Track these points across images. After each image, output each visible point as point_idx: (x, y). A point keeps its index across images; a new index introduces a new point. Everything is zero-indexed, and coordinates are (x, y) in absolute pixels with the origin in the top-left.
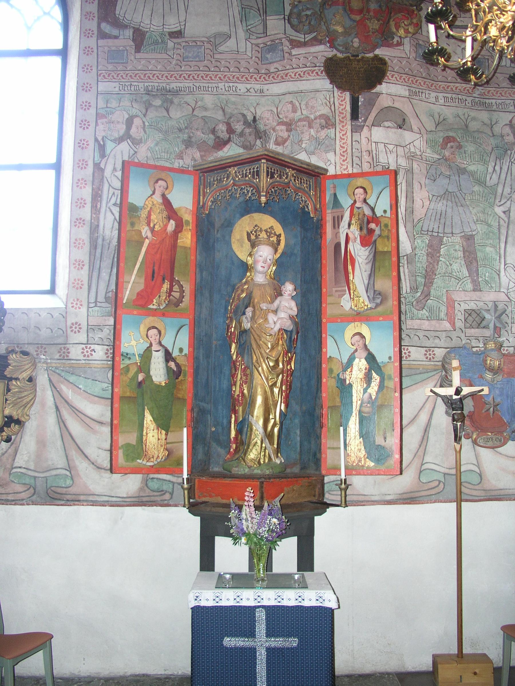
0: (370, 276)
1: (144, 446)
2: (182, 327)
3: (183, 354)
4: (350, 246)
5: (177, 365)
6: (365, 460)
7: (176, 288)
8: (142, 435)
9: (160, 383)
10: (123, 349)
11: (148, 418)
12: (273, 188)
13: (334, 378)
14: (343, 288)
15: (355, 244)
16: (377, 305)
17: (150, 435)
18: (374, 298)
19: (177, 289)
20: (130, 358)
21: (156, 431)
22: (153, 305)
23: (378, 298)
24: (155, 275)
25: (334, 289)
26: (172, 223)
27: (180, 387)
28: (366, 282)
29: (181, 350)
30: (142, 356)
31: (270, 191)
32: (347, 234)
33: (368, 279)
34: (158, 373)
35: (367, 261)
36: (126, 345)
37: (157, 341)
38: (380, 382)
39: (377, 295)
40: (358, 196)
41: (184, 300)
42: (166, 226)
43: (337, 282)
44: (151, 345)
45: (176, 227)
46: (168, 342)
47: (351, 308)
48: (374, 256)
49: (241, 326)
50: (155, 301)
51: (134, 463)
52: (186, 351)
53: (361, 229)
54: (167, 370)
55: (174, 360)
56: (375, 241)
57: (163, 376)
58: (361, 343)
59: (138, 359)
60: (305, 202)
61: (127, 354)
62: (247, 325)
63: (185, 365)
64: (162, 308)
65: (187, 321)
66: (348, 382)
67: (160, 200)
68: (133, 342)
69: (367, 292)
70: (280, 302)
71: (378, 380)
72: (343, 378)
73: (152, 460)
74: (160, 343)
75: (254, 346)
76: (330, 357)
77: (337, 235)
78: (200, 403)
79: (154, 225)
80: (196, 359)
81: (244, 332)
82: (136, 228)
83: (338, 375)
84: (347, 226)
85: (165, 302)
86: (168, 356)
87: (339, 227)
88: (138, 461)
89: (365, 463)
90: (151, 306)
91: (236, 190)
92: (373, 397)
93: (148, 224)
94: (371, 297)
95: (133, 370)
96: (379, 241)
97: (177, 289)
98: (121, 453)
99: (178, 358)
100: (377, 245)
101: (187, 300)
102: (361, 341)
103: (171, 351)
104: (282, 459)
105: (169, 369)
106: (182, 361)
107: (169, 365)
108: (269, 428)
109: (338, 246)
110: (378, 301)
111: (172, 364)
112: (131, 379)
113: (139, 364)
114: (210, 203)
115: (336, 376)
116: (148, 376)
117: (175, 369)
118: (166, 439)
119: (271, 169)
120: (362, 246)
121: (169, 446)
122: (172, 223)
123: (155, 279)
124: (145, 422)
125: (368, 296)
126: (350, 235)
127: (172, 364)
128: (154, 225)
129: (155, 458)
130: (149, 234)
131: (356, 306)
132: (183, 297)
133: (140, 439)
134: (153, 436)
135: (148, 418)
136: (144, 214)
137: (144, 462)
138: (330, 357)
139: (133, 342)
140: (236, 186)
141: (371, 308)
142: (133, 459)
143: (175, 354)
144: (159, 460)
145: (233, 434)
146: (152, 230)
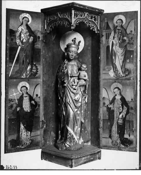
0: (123, 62)
1: (20, 140)
2: (37, 85)
4: (114, 48)
5: (35, 102)
6: (120, 144)
7: (34, 68)
8: (19, 135)
11: (22, 127)
12: (78, 21)
13: (106, 106)
14: (111, 67)
15: (116, 47)
16: (126, 75)
18: (125, 72)
19: (35, 68)
20: (13, 101)
21: (26, 132)
22: (24, 76)
23: (127, 72)
24: (24, 63)
25: (106, 67)
26: (32, 38)
27: (37, 112)
28: (121, 64)
29: (37, 95)
30: (18, 100)
31: (76, 23)
32: (113, 42)
33: (122, 63)
35: (122, 55)
36: (11, 95)
38: (127, 110)
39: (126, 70)
40: (119, 24)
41: (38, 73)
42: (29, 39)
43: (107, 64)
44: (23, 94)
45: (33, 39)
47: (114, 76)
48: (125, 52)
50: (24, 74)
53: (119, 39)
55: (34, 100)
57: (29, 108)
58: (118, 92)
59: (17, 101)
61: (12, 99)
64: (27, 77)
66: (112, 109)
67: (25, 27)
68: (15, 95)
69: (121, 69)
71: (126, 109)
72: (110, 107)
73: (24, 145)
74: (27, 93)
76: (104, 97)
77: (108, 42)
79: (23, 39)
82: (14, 41)
83: (108, 106)
84: (112, 38)
85: (29, 74)
86: (31, 99)
87: (109, 39)
89: (120, 146)
90: (23, 77)
92: (124, 117)
93: (20, 39)
94: (123, 71)
95: (15, 106)
96: (128, 45)
97: (35, 68)
98: (9, 144)
99: (36, 99)
100: (127, 47)
102: (118, 91)
103: (32, 96)
105: (31, 105)
107: (32, 102)
109: (108, 47)
110: (127, 73)
111: (33, 102)
112: (13, 111)
113: (17, 103)
115: (107, 106)
117: (34, 104)
118: (30, 135)
120: (120, 48)
121: (32, 138)
122: (32, 38)
123: (24, 65)
124: (21, 129)
125: (122, 71)
126: (114, 42)
128: (23, 39)
130: (20, 44)
131: (116, 75)
132: (38, 71)
133: (19, 137)
135: (22, 127)
136: (18, 34)
137: (20, 147)
138: (104, 97)
141: (123, 77)
143: (35, 97)
144: (27, 145)
146: (22, 42)
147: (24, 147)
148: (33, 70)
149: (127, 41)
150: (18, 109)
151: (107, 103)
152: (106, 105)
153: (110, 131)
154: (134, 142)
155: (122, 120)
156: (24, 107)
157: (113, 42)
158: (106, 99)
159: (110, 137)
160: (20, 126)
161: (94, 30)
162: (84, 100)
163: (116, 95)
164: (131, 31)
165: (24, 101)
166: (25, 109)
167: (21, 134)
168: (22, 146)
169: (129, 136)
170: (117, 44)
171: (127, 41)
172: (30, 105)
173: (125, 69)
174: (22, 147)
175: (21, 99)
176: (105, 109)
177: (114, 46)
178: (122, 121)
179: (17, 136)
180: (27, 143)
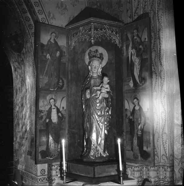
3: (64, 109)
7: (61, 81)
9: (55, 122)
10: (40, 109)
17: (51, 146)
20: (43, 113)
32: (131, 52)
34: (54, 118)
37: (54, 104)
43: (128, 76)
46: (58, 104)
49: (86, 97)
51: (45, 159)
52: (65, 108)
54: (58, 118)
55: (61, 112)
56: (142, 54)
60: (115, 40)
61: (42, 110)
62: (88, 96)
63: (65, 115)
65: (65, 95)
66: (132, 120)
70: (102, 85)
74: (55, 105)
75: (91, 105)
76: (126, 109)
78: (72, 130)
80: (70, 111)
81: (87, 100)
83: (129, 117)
86: (58, 111)
88: (47, 158)
91: (83, 37)
92: (142, 128)
95: (44, 118)
101: (65, 85)
102: (137, 102)
103: (59, 108)
104: (107, 154)
105: (59, 117)
106: (63, 112)
108: (99, 142)
114: (73, 44)
116: (50, 120)
119: (97, 26)
126: (133, 53)
127: (60, 114)
129: (54, 156)
132: (64, 85)
134: (53, 146)
137: (49, 158)
138: (126, 109)
139: (43, 106)
140: (83, 35)
142: (45, 157)
143: (61, 109)
145: (85, 144)
147: (52, 158)
148: (60, 84)
149: (142, 49)
150: (47, 121)
151: (129, 114)
152: (128, 116)
153: (132, 143)
154: (152, 155)
155: (141, 131)
156: (52, 118)
157: (131, 52)
158: (128, 110)
159: (132, 150)
160: (49, 138)
161: (115, 43)
162: (108, 112)
163: (135, 106)
164: (145, 39)
165: (52, 113)
166: (53, 121)
167: (50, 145)
168: (51, 157)
169: (147, 149)
170: (134, 54)
171: (142, 49)
172: (57, 117)
173: (142, 78)
174: (51, 159)
175: (50, 112)
176: (127, 120)
177: (133, 57)
178: (141, 132)
179: (46, 147)
180: (55, 155)
